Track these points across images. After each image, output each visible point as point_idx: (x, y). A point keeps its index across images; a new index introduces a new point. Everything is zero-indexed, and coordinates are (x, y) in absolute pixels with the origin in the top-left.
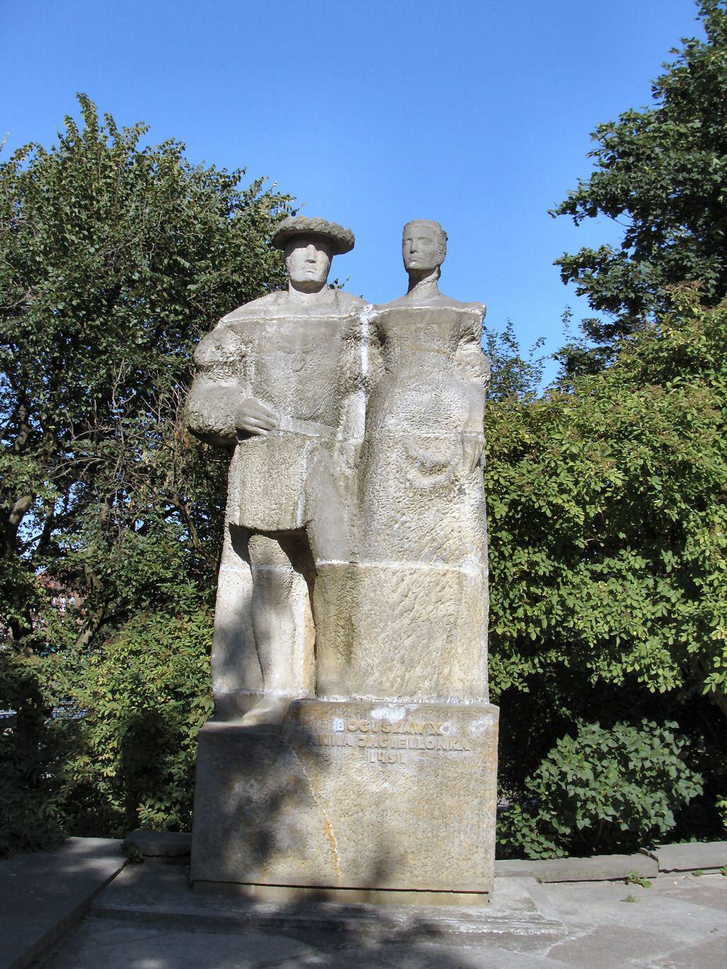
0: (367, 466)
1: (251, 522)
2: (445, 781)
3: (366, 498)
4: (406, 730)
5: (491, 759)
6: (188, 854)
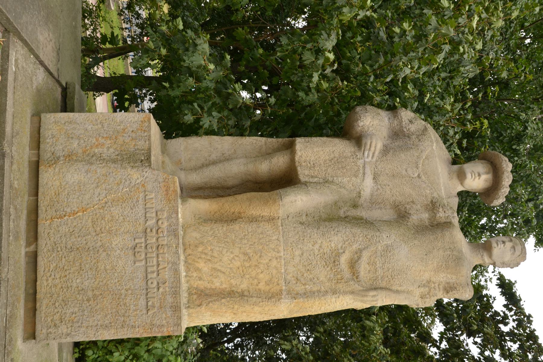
0: (349, 222)
1: (299, 149)
2: (123, 296)
3: (327, 223)
4: (161, 263)
5: (141, 331)
6: (65, 111)
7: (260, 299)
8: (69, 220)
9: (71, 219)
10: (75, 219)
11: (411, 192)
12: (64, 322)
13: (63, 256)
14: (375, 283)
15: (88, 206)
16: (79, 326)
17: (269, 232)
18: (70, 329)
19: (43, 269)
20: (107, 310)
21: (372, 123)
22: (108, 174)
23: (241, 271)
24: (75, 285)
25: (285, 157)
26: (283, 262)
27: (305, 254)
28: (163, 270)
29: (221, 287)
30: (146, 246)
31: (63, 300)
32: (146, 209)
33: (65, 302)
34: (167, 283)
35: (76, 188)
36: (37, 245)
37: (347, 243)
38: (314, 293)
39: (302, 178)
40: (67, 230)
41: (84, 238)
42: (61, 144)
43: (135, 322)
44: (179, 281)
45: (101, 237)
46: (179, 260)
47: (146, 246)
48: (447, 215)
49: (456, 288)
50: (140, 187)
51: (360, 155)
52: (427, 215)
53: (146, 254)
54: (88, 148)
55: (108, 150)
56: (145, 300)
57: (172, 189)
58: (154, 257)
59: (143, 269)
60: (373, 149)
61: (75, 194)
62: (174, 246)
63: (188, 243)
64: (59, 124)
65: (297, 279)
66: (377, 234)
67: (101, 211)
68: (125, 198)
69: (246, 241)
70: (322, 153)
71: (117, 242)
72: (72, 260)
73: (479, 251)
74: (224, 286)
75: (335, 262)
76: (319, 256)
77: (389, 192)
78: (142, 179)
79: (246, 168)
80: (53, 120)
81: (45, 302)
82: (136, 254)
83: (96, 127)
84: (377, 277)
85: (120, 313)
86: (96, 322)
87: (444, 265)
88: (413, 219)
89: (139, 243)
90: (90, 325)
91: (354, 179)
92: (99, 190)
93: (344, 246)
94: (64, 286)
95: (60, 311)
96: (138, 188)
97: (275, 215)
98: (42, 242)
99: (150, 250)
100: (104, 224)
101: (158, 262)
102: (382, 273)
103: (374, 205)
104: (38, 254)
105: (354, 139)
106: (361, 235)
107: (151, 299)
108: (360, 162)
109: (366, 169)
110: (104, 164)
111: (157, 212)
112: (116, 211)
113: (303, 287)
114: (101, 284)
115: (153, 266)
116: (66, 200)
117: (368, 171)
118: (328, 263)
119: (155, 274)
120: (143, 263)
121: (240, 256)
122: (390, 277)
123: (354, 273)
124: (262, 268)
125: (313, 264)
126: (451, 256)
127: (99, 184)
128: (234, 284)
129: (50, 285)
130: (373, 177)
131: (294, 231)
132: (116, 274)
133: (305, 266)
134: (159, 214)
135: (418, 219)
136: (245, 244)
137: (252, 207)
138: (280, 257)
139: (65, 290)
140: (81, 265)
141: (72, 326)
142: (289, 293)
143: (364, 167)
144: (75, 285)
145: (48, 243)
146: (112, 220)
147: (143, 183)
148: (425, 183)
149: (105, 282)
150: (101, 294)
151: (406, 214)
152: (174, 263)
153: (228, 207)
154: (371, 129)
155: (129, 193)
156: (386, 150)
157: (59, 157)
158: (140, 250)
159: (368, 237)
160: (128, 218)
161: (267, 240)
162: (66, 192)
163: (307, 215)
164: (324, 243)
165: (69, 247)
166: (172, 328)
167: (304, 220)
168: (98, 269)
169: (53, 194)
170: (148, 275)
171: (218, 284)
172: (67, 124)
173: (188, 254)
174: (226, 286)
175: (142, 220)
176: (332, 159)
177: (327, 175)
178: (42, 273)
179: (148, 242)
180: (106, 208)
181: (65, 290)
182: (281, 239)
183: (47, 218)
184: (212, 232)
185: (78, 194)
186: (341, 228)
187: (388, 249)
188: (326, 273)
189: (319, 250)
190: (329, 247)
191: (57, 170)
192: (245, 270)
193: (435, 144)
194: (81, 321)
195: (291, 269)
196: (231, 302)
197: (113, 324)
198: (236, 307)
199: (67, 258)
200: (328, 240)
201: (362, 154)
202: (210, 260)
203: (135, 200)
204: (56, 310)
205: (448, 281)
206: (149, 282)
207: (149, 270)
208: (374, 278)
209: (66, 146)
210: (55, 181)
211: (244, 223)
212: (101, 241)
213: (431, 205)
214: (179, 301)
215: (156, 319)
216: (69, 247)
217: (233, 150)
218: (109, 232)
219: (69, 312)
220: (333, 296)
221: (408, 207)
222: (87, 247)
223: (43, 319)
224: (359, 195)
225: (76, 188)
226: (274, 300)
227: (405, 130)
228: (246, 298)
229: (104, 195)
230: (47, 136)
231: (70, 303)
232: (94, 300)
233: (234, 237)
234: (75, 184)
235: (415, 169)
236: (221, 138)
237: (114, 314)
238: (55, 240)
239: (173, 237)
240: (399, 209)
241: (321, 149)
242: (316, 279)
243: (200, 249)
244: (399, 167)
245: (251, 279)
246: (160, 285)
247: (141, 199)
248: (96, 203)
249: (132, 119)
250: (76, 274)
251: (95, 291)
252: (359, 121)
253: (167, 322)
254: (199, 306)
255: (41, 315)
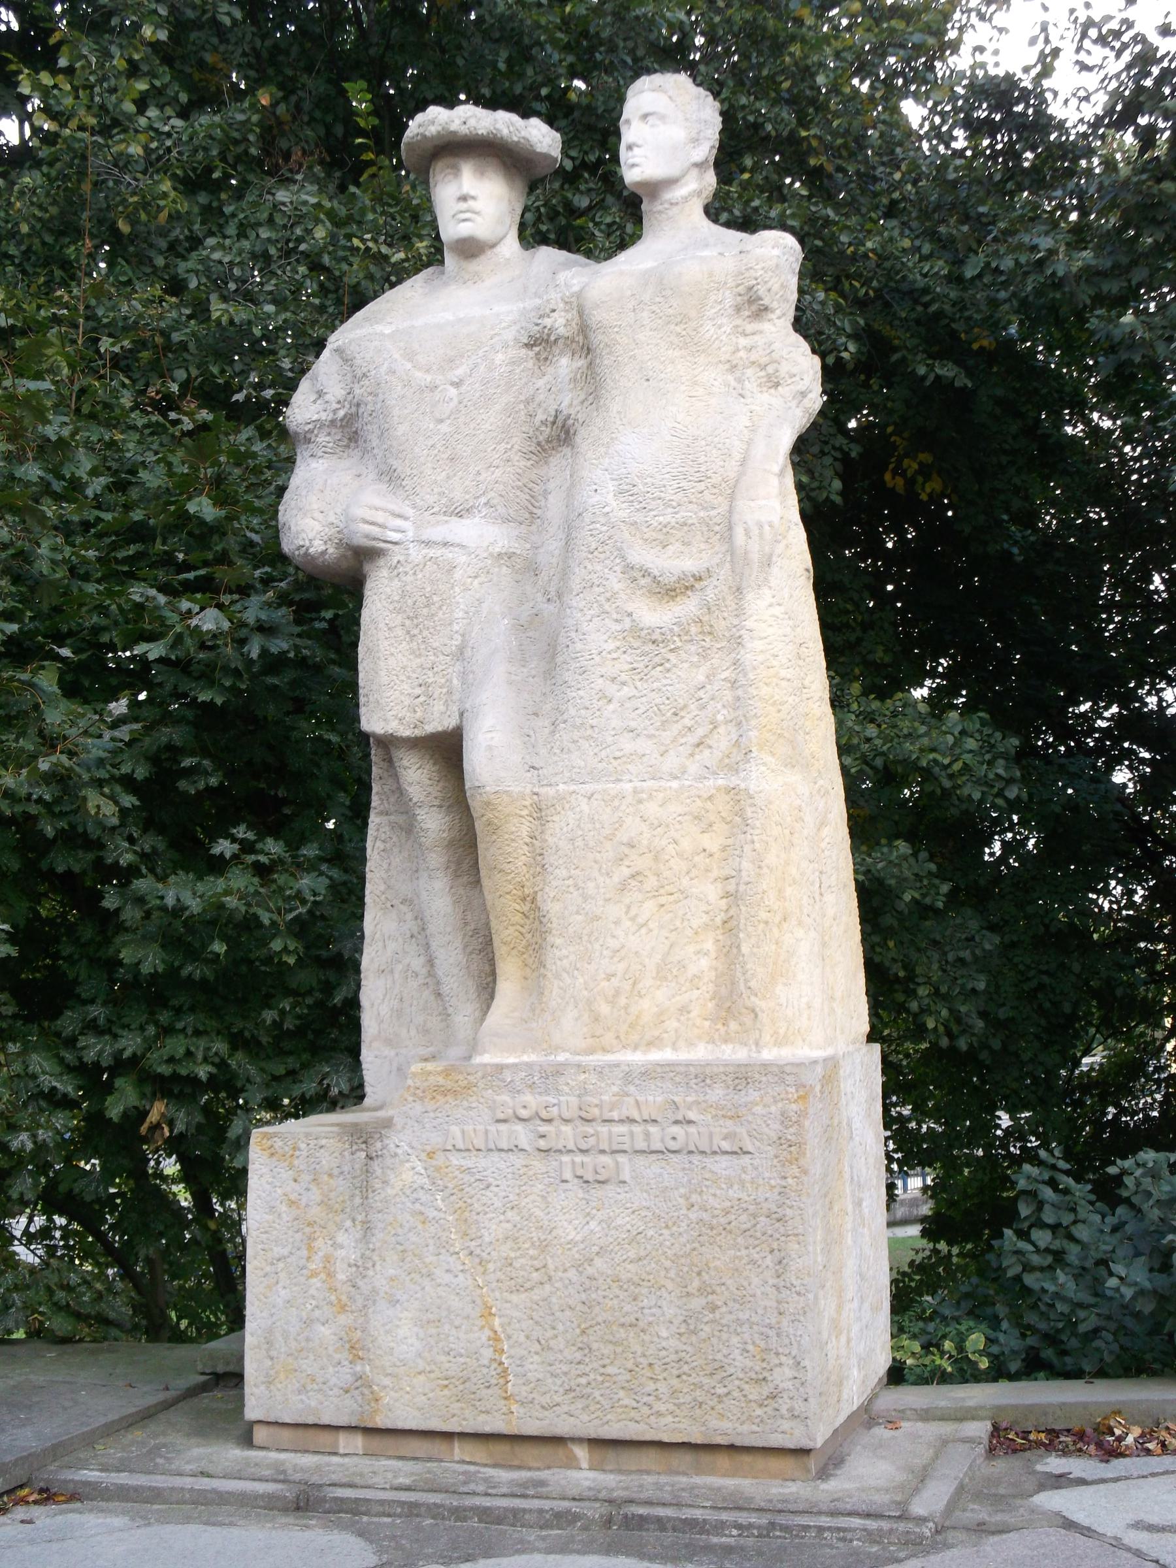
1: (382, 724)
2: (705, 1216)
3: (559, 659)
4: (625, 1113)
7: (747, 848)
8: (512, 1352)
9: (511, 1347)
10: (509, 1337)
11: (497, 407)
12: (766, 1374)
13: (602, 1370)
14: (717, 528)
15: (479, 1301)
16: (778, 1335)
17: (571, 822)
18: (783, 1359)
19: (632, 1425)
20: (740, 1258)
21: (317, 515)
22: (400, 1248)
23: (671, 898)
24: (673, 1343)
25: (405, 763)
26: (650, 783)
27: (633, 724)
28: (643, 1107)
29: (713, 955)
30: (581, 1151)
31: (712, 1374)
32: (490, 1150)
33: (717, 1369)
34: (676, 1099)
35: (433, 1331)
36: (573, 1440)
37: (607, 607)
38: (738, 699)
39: (450, 723)
40: (536, 1358)
41: (558, 1314)
42: (322, 1368)
43: (773, 1187)
44: (671, 1066)
45: (556, 1269)
46: (617, 1065)
47: (581, 1151)
48: (562, 305)
49: (750, 288)
50: (434, 1163)
51: (396, 554)
52: (564, 361)
53: (603, 1152)
54: (333, 1298)
55: (342, 1247)
56: (717, 1158)
57: (441, 1080)
58: (610, 1132)
59: (641, 1161)
60: (380, 517)
61: (448, 1336)
62: (583, 1076)
63: (590, 1041)
64: (272, 1372)
65: (698, 745)
66: (587, 520)
67: (491, 1266)
68: (461, 1204)
69: (591, 885)
70: (392, 662)
71: (570, 1228)
72: (611, 1347)
73: (660, 212)
74: (709, 945)
75: (655, 639)
76: (638, 684)
77: (498, 472)
78: (413, 1158)
79: (440, 874)
80: (263, 1388)
81: (714, 1423)
82: (600, 1178)
83: (282, 1275)
84: (702, 521)
85: (748, 1225)
86: (768, 1289)
87: (678, 329)
88: (571, 405)
89: (574, 1170)
90: (775, 1304)
91: (458, 574)
92: (438, 1272)
93: (615, 616)
94: (675, 1372)
95: (737, 1382)
96: (438, 1169)
97: (527, 803)
98: (563, 1427)
99: (592, 1141)
100: (522, 1261)
101: (621, 1121)
102: (691, 506)
103: (539, 512)
104: (593, 1436)
105: (361, 563)
106: (589, 567)
107: (715, 1142)
108: (416, 554)
109: (434, 538)
110: (376, 1258)
111: (498, 1121)
112: (493, 1229)
113: (722, 730)
114: (672, 1274)
115: (632, 1134)
116: (462, 1360)
117: (436, 533)
118: (657, 660)
119: (653, 1129)
120: (622, 1158)
121: (627, 901)
122: (701, 486)
123: (687, 588)
124: (664, 842)
125: (658, 701)
126: (654, 308)
127: (424, 1271)
128: (705, 918)
129: (671, 1407)
130: (454, 519)
131: (569, 751)
132: (651, 1233)
133: (663, 723)
134: (501, 1116)
135: (571, 390)
136: (598, 887)
137: (506, 867)
138: (635, 791)
139: (686, 1368)
140: (623, 1325)
141: (777, 1354)
142: (734, 769)
143: (428, 543)
144: (673, 1343)
145: (565, 1408)
146: (515, 1240)
147: (423, 1156)
148: (476, 365)
149: (668, 1264)
150: (699, 1274)
151: (559, 423)
152: (628, 1078)
153: (511, 929)
154: (332, 519)
155: (448, 1192)
156: (390, 477)
157: (354, 1374)
158: (591, 1168)
159: (594, 546)
160: (512, 1197)
161: (590, 826)
162: (443, 1358)
163: (536, 714)
164: (603, 671)
165: (578, 1356)
166: (790, 1089)
167: (547, 723)
168: (636, 1279)
169: (446, 1392)
170: (653, 1148)
171: (704, 963)
172: (273, 1353)
173: (615, 1042)
174: (711, 941)
175: (517, 1160)
176: (408, 632)
177: (447, 650)
178: (641, 1427)
179: (571, 1146)
180: (484, 1255)
181: (686, 1368)
182: (589, 788)
183: (505, 1409)
184: (565, 975)
185: (447, 1327)
186: (571, 622)
187: (626, 491)
188: (686, 665)
189: (624, 684)
190: (615, 655)
191: (387, 1381)
192: (668, 888)
193: (379, 328)
194: (764, 1330)
195: (671, 762)
196: (750, 929)
197: (775, 1245)
198: (763, 915)
199: (607, 1361)
200: (597, 659)
201: (396, 548)
202: (634, 983)
203: (467, 1178)
204: (736, 1394)
205: (730, 311)
206: (673, 1145)
207: (641, 1145)
208: (705, 529)
209: (329, 1356)
210: (413, 1388)
211: (547, 889)
212: (565, 1271)
213: (537, 349)
214: (722, 1069)
215: (766, 1130)
216: (578, 1356)
217: (404, 908)
218: (544, 1246)
219: (740, 1361)
220: (749, 645)
221: (541, 416)
222: (580, 1307)
223: (755, 1428)
224: (507, 557)
225: (433, 1331)
226: (749, 811)
227: (341, 413)
228: (742, 888)
229: (452, 1259)
230: (301, 1406)
231: (719, 1356)
232: (713, 1292)
233: (579, 918)
234: (422, 1335)
235: (437, 395)
236: (367, 941)
237: (751, 1241)
238: (561, 1390)
239: (562, 1080)
240: (548, 441)
241: (382, 663)
242: (701, 693)
243: (604, 1009)
244: (430, 443)
245: (694, 873)
246: (680, 1118)
247: (463, 1162)
248: (470, 1282)
249: (263, 1180)
250: (647, 1338)
251: (690, 1289)
252: (311, 550)
253: (775, 1102)
254: (756, 1016)
255: (745, 1434)
